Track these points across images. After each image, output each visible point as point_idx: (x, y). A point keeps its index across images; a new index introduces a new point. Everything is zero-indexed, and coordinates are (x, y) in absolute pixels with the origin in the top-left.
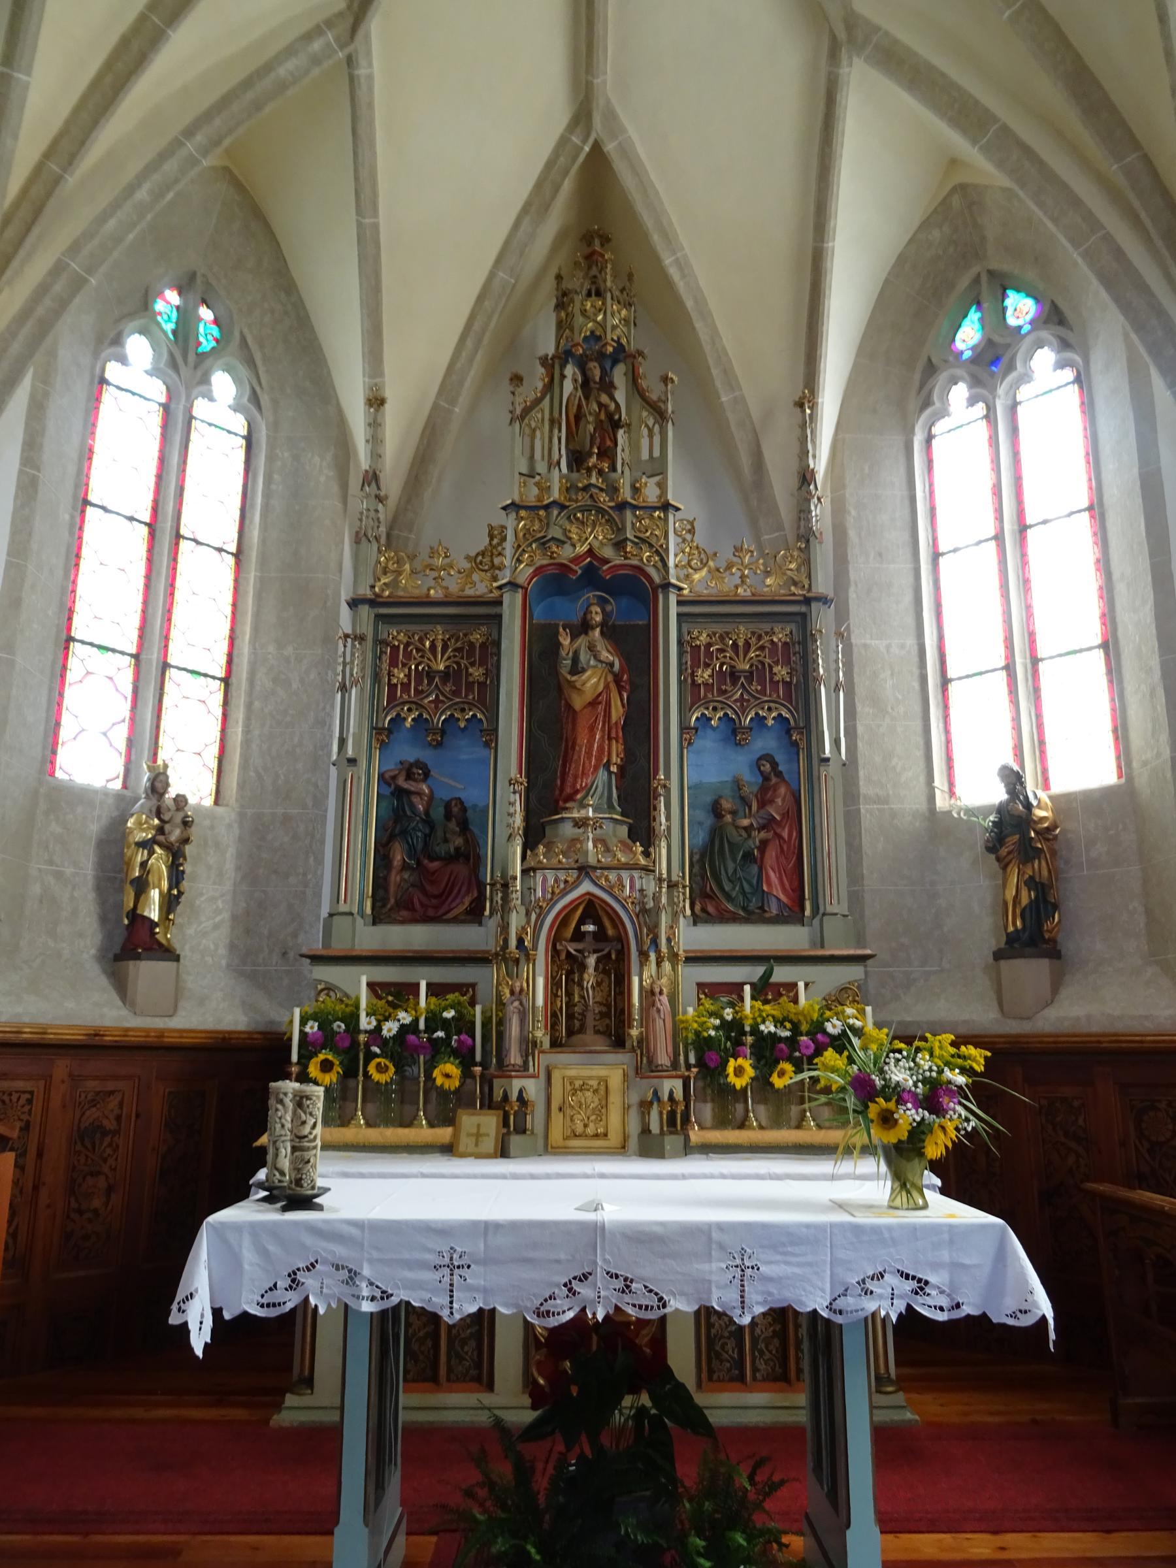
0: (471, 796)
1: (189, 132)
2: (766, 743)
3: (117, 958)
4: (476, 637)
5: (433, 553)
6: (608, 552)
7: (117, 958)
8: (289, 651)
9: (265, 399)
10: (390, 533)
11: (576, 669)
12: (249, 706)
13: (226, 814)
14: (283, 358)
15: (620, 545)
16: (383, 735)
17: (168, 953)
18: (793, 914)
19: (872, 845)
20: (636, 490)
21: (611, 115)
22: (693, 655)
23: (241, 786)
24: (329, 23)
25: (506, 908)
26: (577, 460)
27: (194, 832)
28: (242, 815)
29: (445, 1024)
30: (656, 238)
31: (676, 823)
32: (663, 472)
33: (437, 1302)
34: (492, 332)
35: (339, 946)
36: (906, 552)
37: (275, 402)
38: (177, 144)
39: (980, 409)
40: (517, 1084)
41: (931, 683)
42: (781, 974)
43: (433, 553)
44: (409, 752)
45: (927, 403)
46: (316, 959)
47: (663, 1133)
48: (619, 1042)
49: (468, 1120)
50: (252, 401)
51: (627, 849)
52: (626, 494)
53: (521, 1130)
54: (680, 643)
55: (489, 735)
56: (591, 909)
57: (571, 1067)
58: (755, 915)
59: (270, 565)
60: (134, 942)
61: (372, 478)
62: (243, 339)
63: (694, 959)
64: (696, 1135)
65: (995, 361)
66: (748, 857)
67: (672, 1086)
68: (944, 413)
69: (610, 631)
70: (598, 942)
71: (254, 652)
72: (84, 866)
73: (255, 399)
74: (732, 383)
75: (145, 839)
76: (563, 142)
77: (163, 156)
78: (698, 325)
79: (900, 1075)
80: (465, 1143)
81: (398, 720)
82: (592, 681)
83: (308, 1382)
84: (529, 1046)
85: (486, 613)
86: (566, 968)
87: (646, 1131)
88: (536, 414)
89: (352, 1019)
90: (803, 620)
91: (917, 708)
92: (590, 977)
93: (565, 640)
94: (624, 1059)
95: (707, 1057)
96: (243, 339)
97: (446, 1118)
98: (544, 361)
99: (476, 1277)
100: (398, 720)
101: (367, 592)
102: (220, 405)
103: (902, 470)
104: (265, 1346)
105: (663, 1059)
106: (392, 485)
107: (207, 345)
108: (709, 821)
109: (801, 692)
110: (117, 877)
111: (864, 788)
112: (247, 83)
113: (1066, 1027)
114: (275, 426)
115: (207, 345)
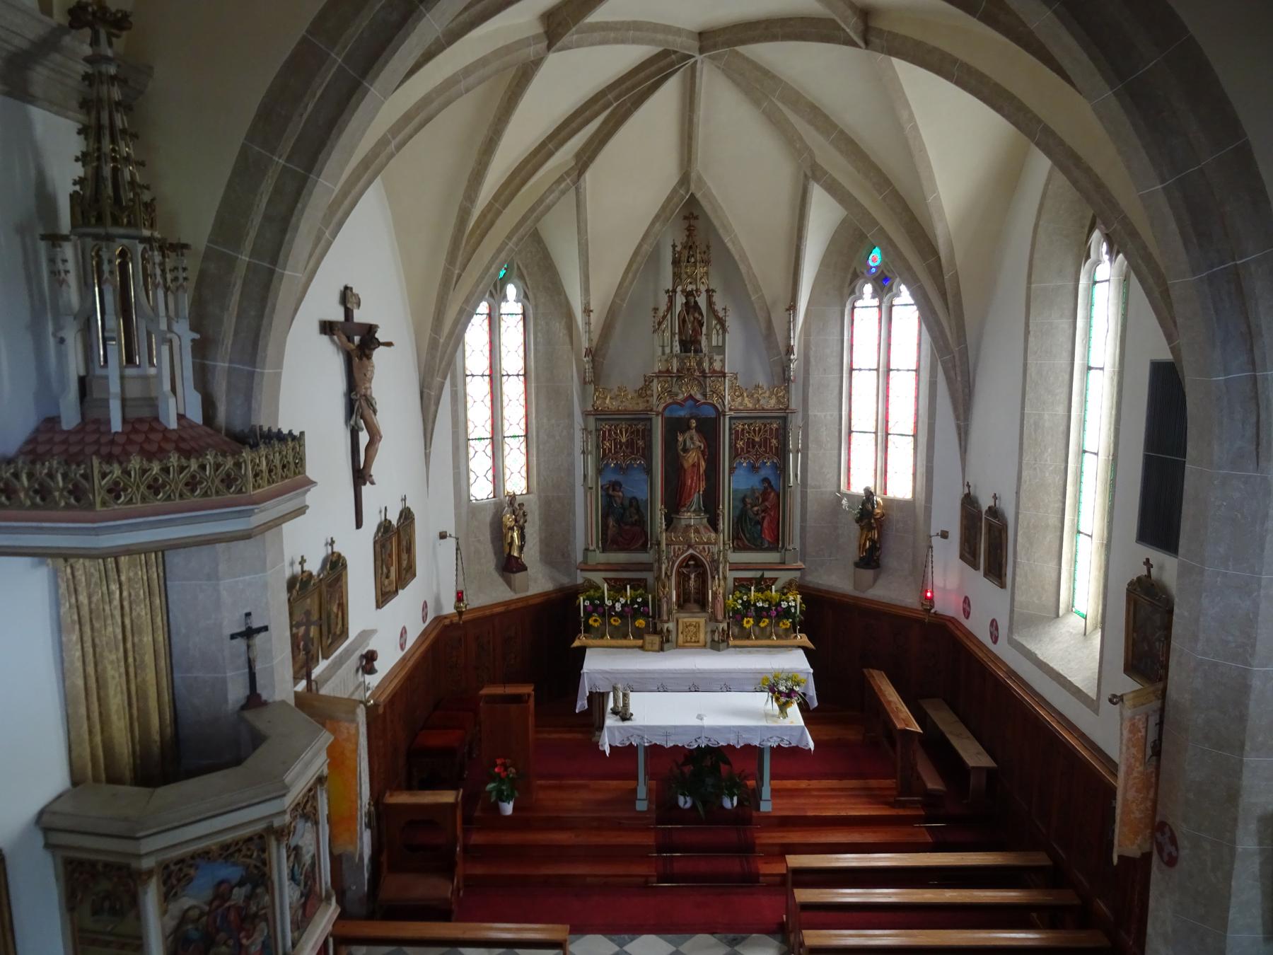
1: (509, 237)
6: (699, 397)
8: (553, 421)
9: (530, 295)
11: (685, 450)
12: (538, 448)
14: (540, 277)
15: (705, 395)
16: (599, 472)
17: (524, 568)
18: (773, 547)
19: (812, 506)
21: (700, 178)
23: (538, 484)
24: (568, 173)
27: (528, 518)
28: (539, 497)
30: (721, 231)
32: (724, 353)
33: (663, 743)
36: (837, 369)
37: (535, 298)
38: (504, 244)
40: (666, 626)
44: (614, 478)
45: (853, 292)
47: (718, 643)
49: (648, 638)
50: (524, 297)
53: (668, 641)
54: (730, 429)
57: (685, 618)
58: (759, 548)
59: (540, 376)
60: (510, 566)
62: (519, 268)
64: (732, 642)
65: (883, 284)
66: (758, 523)
68: (861, 297)
70: (696, 573)
71: (537, 422)
72: (486, 536)
73: (526, 296)
74: (757, 289)
75: (501, 528)
76: (674, 191)
80: (648, 646)
86: (683, 578)
87: (713, 640)
89: (602, 598)
90: (785, 419)
91: (836, 445)
92: (692, 583)
95: (737, 616)
96: (519, 268)
97: (641, 637)
98: (667, 291)
99: (673, 738)
100: (607, 465)
101: (590, 408)
102: (512, 305)
103: (838, 328)
104: (625, 753)
108: (741, 506)
109: (782, 453)
110: (499, 533)
111: (809, 482)
112: (532, 209)
113: (875, 598)
114: (536, 307)
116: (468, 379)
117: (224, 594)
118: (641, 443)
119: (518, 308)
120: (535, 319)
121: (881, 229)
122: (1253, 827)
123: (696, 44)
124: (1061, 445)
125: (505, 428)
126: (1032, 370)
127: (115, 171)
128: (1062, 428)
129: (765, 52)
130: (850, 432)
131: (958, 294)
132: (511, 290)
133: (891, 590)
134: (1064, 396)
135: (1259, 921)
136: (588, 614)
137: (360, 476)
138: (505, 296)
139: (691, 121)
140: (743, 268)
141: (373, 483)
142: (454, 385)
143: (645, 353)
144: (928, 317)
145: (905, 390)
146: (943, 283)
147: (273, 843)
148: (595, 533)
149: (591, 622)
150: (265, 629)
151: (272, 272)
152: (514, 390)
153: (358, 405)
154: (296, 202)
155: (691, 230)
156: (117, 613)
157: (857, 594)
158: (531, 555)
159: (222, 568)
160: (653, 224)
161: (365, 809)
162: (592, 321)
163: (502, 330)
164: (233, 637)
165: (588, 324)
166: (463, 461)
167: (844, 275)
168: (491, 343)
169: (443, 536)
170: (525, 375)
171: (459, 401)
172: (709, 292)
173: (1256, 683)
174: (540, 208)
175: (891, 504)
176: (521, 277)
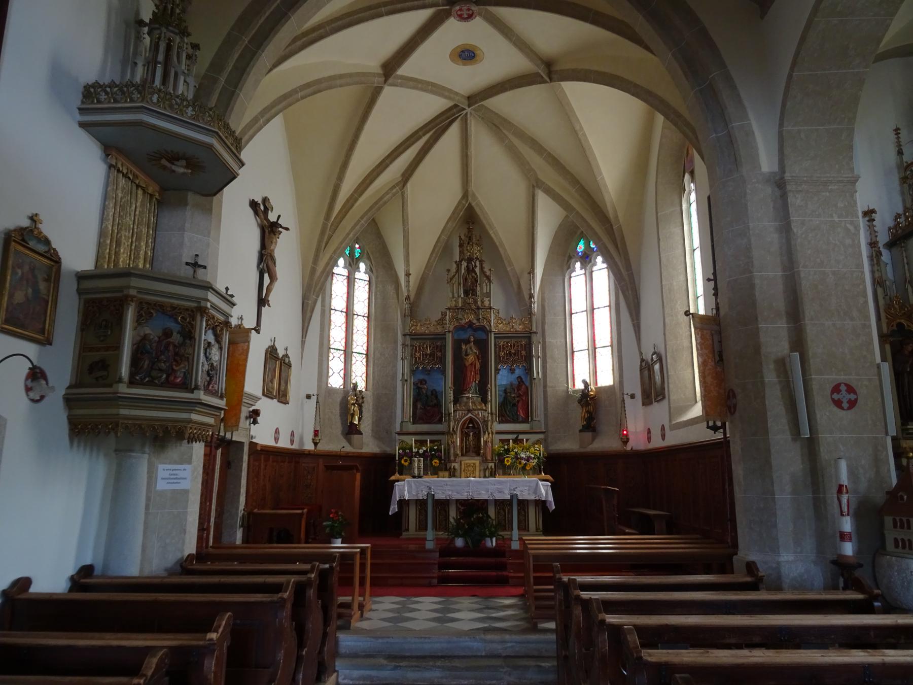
0: (438, 389)
1: (362, 218)
2: (518, 372)
3: (347, 434)
4: (439, 344)
5: (426, 320)
6: (475, 321)
7: (347, 434)
9: (374, 270)
10: (412, 310)
11: (467, 355)
13: (369, 393)
15: (478, 320)
16: (413, 372)
17: (360, 433)
18: (525, 421)
19: (550, 400)
20: (482, 302)
21: (474, 195)
22: (498, 348)
24: (397, 184)
25: (449, 421)
26: (466, 293)
29: (434, 450)
30: (487, 227)
31: (494, 396)
34: (442, 250)
35: (405, 430)
37: (377, 270)
38: (359, 221)
39: (583, 272)
40: (453, 465)
41: (568, 353)
42: (521, 437)
43: (426, 320)
44: (421, 377)
45: (569, 267)
46: (399, 434)
48: (478, 454)
50: (370, 271)
51: (480, 404)
52: (479, 303)
54: (495, 345)
55: (443, 372)
56: (471, 420)
57: (466, 461)
58: (515, 420)
60: (351, 430)
61: (408, 298)
63: (498, 433)
65: (586, 259)
66: (514, 405)
67: (491, 465)
68: (574, 270)
69: (475, 342)
70: (473, 429)
72: (337, 410)
73: (371, 270)
74: (511, 264)
75: (349, 400)
76: (460, 202)
77: (356, 225)
78: (500, 249)
79: (523, 456)
81: (417, 368)
82: (471, 358)
83: (408, 530)
84: (456, 455)
85: (442, 337)
86: (465, 436)
88: (454, 280)
89: (411, 449)
90: (530, 338)
92: (471, 438)
93: (463, 347)
94: (479, 458)
100: (417, 368)
101: (407, 331)
102: (362, 274)
105: (489, 458)
106: (412, 298)
107: (357, 255)
108: (503, 395)
109: (528, 359)
111: (548, 384)
112: (376, 203)
114: (377, 277)
115: (357, 255)
116: (333, 312)
117: (186, 239)
118: (439, 354)
119: (366, 277)
120: (376, 284)
121: (578, 212)
122: (772, 366)
123: (466, 102)
124: (685, 298)
125: (354, 346)
126: (664, 260)
127: (172, 8)
128: (684, 288)
129: (499, 103)
130: (573, 352)
131: (624, 243)
132: (362, 266)
133: (606, 443)
134: (683, 270)
135: (787, 427)
136: (400, 459)
137: (262, 302)
138: (358, 268)
139: (467, 156)
140: (502, 252)
141: (269, 306)
142: (323, 301)
143: (442, 301)
144: (613, 267)
145: (604, 319)
146: (614, 234)
147: (199, 318)
148: (409, 411)
149: (403, 462)
150: (205, 267)
151: (234, 92)
152: (360, 325)
153: (266, 262)
154: (251, 61)
155: (469, 223)
156: (133, 214)
157: (582, 450)
158: (366, 427)
159: (187, 225)
160: (447, 223)
161: (240, 514)
162: (411, 284)
163: (356, 287)
164: (187, 264)
165: (408, 282)
166: (326, 329)
167: (564, 258)
168: (348, 293)
169: (309, 397)
170: (368, 317)
171: (327, 311)
172: (481, 262)
173: (757, 281)
174: (379, 204)
175: (600, 390)
176: (369, 258)
